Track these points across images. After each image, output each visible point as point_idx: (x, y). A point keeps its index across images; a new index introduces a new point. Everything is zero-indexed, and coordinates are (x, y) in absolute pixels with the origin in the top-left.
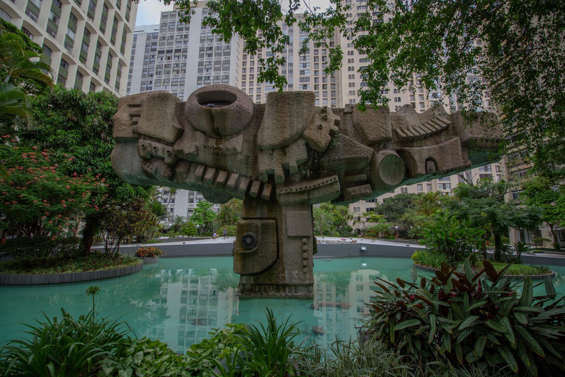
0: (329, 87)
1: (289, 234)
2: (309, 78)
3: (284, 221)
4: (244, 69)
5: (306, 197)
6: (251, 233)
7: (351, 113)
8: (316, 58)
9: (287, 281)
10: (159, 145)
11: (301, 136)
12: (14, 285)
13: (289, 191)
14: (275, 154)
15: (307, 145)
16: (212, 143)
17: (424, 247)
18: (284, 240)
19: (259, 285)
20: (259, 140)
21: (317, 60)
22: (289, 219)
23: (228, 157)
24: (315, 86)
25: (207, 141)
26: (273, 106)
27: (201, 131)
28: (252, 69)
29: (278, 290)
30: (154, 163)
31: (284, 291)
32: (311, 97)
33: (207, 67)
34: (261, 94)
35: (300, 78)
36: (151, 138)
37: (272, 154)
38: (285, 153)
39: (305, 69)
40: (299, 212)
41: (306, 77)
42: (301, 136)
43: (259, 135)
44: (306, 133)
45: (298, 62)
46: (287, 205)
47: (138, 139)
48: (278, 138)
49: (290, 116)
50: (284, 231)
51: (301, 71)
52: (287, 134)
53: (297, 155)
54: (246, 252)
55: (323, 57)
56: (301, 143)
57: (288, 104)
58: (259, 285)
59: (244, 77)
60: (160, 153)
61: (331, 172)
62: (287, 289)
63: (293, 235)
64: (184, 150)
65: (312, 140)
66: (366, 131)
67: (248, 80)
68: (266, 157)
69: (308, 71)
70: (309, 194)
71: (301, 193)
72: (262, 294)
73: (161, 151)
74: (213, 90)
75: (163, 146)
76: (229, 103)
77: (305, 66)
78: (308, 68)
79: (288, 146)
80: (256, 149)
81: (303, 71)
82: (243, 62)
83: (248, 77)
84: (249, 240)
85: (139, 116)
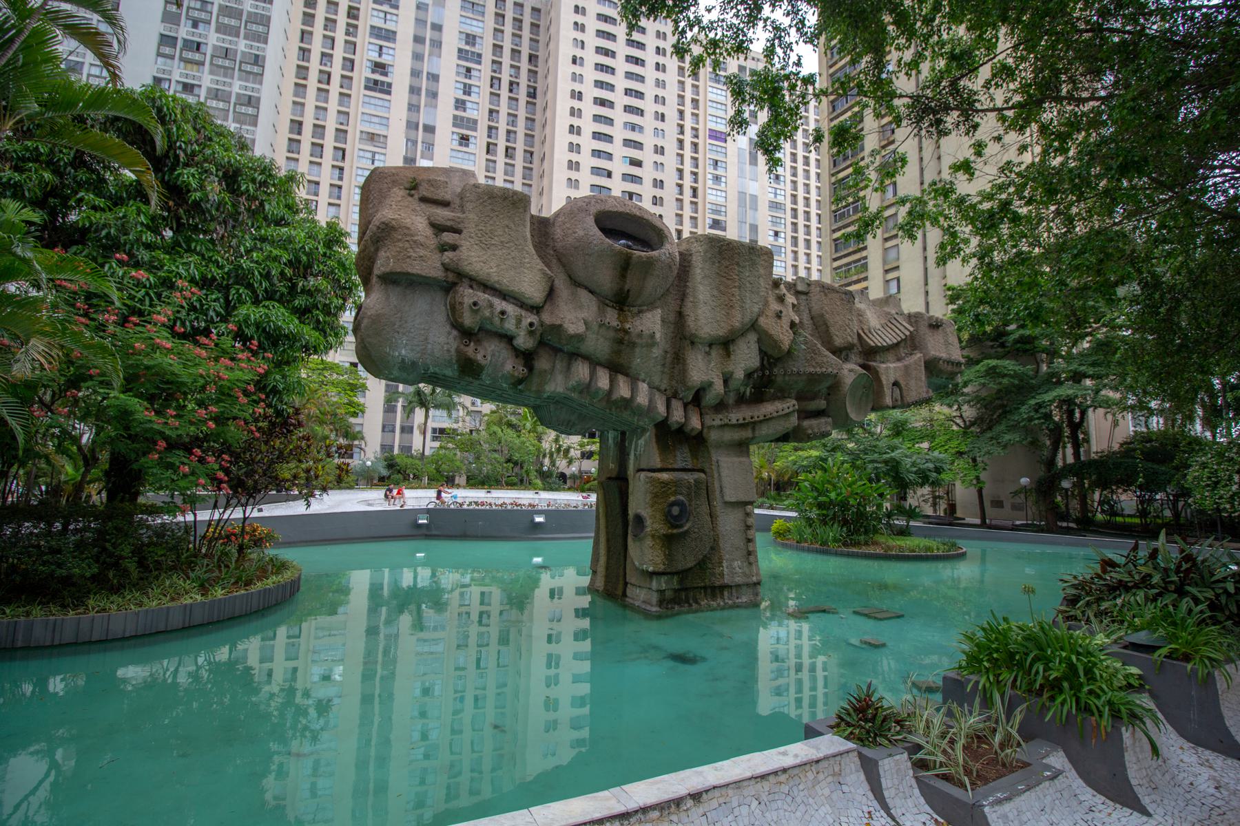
0: (519, 154)
1: (727, 499)
2: (475, 122)
3: (716, 475)
4: (305, 53)
5: (748, 433)
6: (681, 498)
7: (806, 294)
8: (495, 81)
9: (727, 580)
10: (510, 309)
11: (753, 326)
12: (52, 646)
13: (726, 421)
14: (714, 353)
15: (759, 341)
16: (612, 317)
17: (794, 514)
18: (718, 508)
19: (686, 589)
20: (691, 322)
21: (496, 86)
22: (725, 472)
23: (637, 350)
24: (489, 144)
25: (601, 312)
26: (713, 263)
27: (586, 288)
28: (326, 57)
29: (714, 597)
30: (486, 344)
31: (722, 597)
32: (767, 256)
33: (196, 14)
34: (350, 129)
35: (455, 117)
36: (486, 286)
37: (708, 354)
38: (728, 354)
39: (466, 98)
40: (736, 459)
41: (468, 119)
42: (753, 326)
43: (688, 310)
44: (762, 321)
45: (453, 77)
46: (720, 445)
47: (455, 284)
48: (723, 324)
49: (740, 287)
50: (717, 492)
51: (457, 101)
52: (737, 320)
53: (746, 357)
54: (675, 531)
55: (511, 83)
56: (752, 337)
57: (738, 264)
58: (686, 589)
59: (302, 71)
60: (510, 325)
61: (781, 395)
62: (726, 593)
63: (733, 500)
64: (565, 326)
65: (770, 336)
66: (832, 330)
67: (312, 83)
68: (700, 357)
69: (475, 106)
70: (754, 429)
71: (742, 426)
72: (690, 605)
73: (514, 321)
74: (621, 210)
75: (518, 311)
76: (647, 244)
77: (467, 90)
78: (474, 97)
79: (733, 340)
80: (681, 337)
81: (464, 102)
82: (303, 32)
83: (313, 76)
84: (676, 511)
85: (459, 232)
